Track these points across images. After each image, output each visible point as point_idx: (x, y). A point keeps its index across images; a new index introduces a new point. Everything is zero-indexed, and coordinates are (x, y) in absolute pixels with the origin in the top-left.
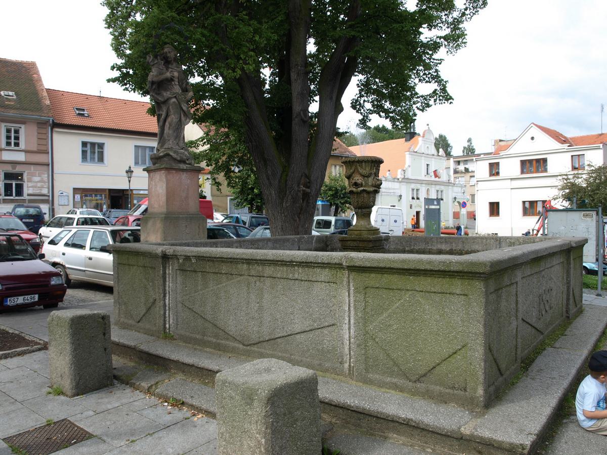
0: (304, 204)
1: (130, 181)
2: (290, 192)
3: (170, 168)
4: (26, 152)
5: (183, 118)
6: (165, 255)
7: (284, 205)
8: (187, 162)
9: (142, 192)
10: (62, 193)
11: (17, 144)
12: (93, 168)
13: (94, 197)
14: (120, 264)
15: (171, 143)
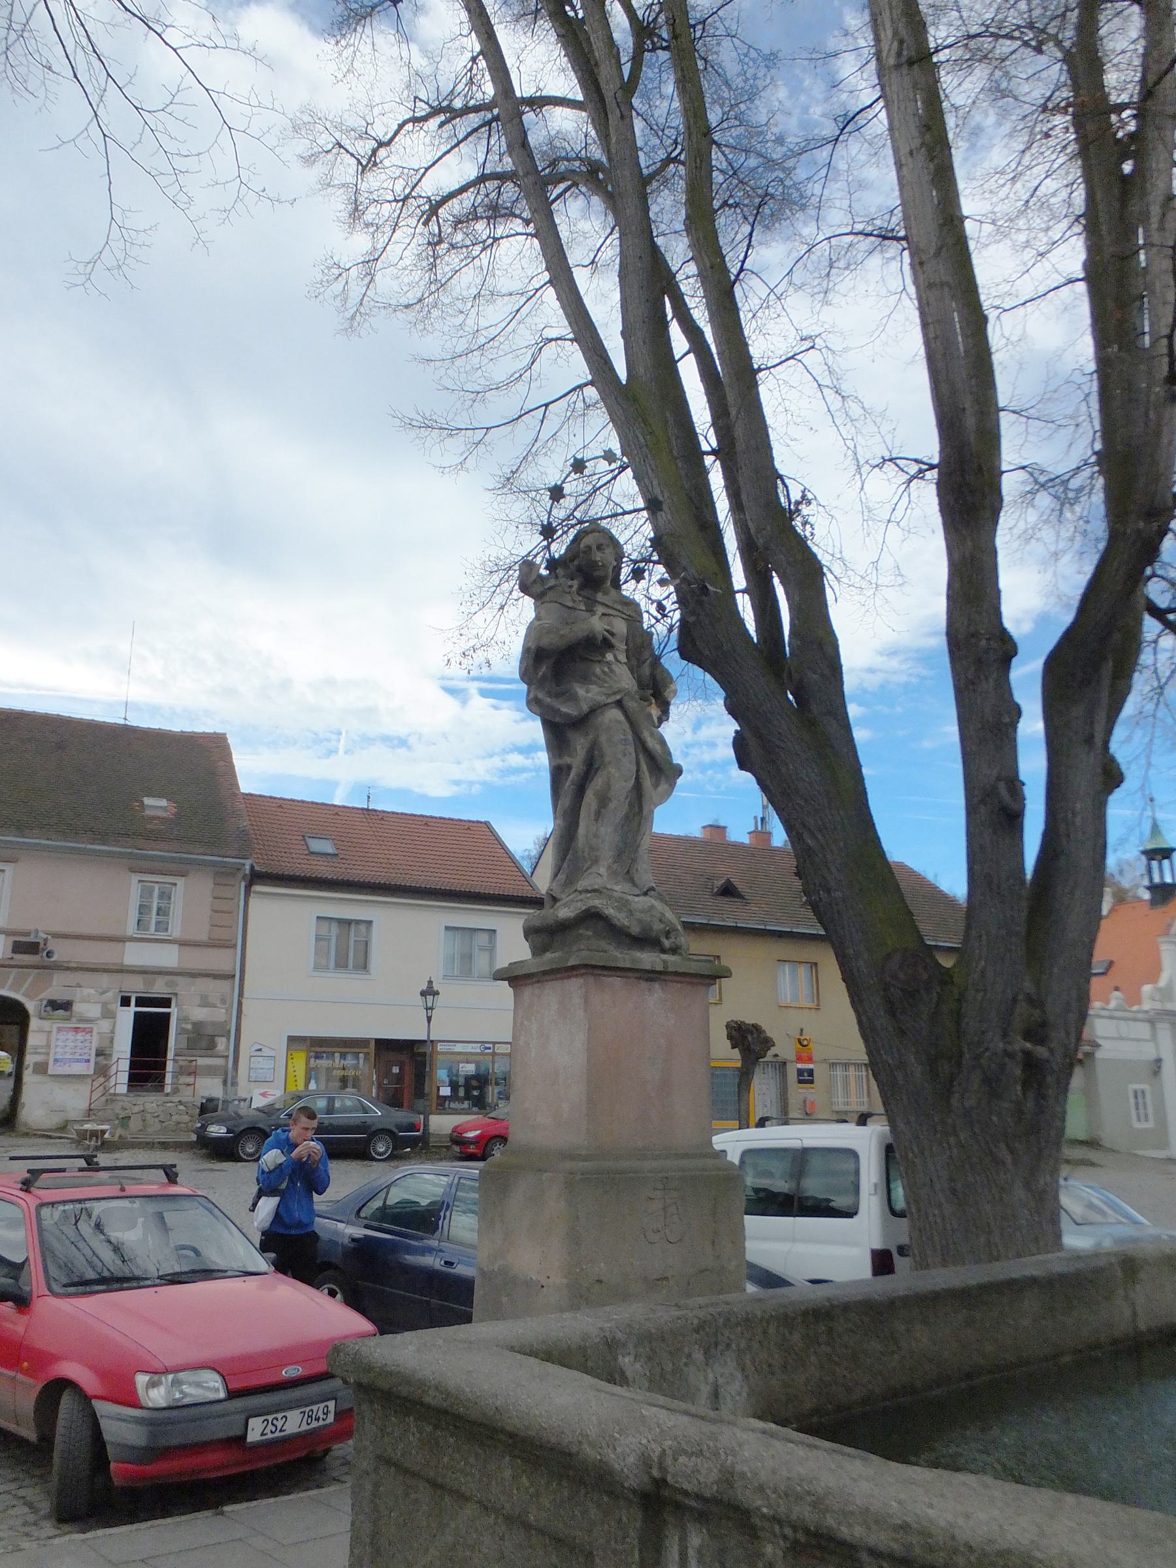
0: (1030, 1105)
1: (429, 1019)
2: (977, 1057)
3: (604, 968)
4: (183, 944)
5: (647, 782)
6: (660, 1483)
7: (955, 1101)
8: (667, 943)
9: (459, 1048)
10: (260, 1050)
11: (162, 926)
12: (348, 984)
13: (337, 1060)
14: (389, 1462)
15: (602, 870)
